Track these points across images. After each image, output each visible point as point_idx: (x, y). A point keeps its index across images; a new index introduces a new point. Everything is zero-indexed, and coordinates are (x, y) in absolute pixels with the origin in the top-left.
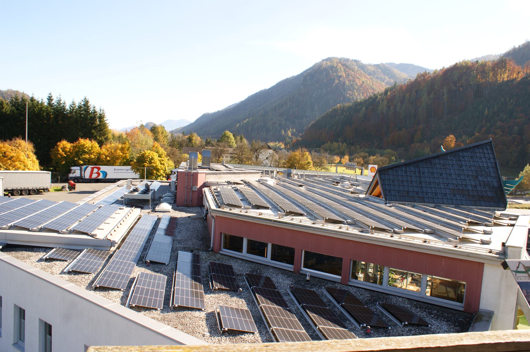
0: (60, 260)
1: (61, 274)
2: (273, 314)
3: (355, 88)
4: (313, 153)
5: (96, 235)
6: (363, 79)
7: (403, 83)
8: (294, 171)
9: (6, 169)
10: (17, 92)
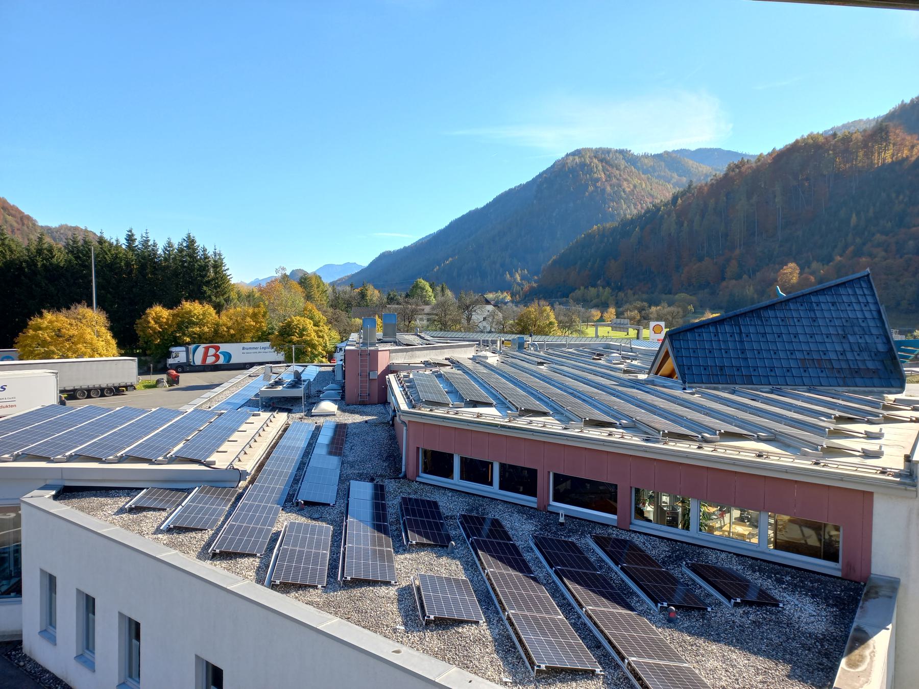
0: (154, 509)
1: (154, 533)
2: (508, 587)
3: (622, 198)
4: (557, 306)
5: (214, 463)
6: (634, 182)
7: (703, 182)
8: (529, 340)
9: (63, 357)
10: (76, 228)
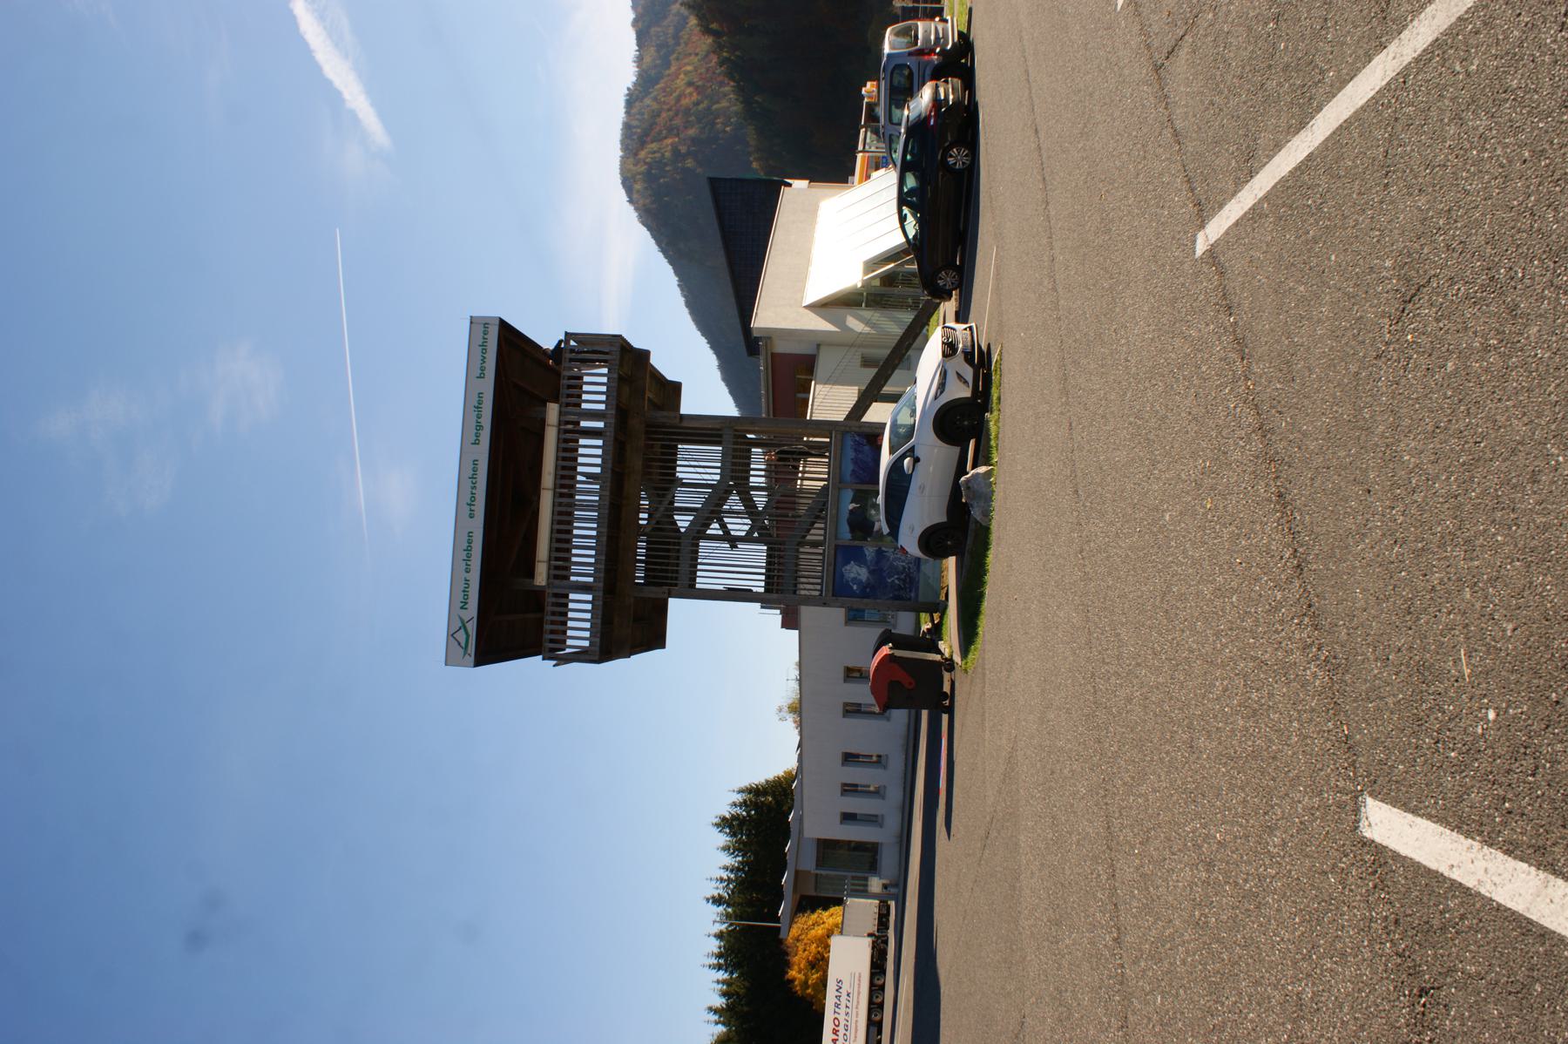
3: (709, 108)
